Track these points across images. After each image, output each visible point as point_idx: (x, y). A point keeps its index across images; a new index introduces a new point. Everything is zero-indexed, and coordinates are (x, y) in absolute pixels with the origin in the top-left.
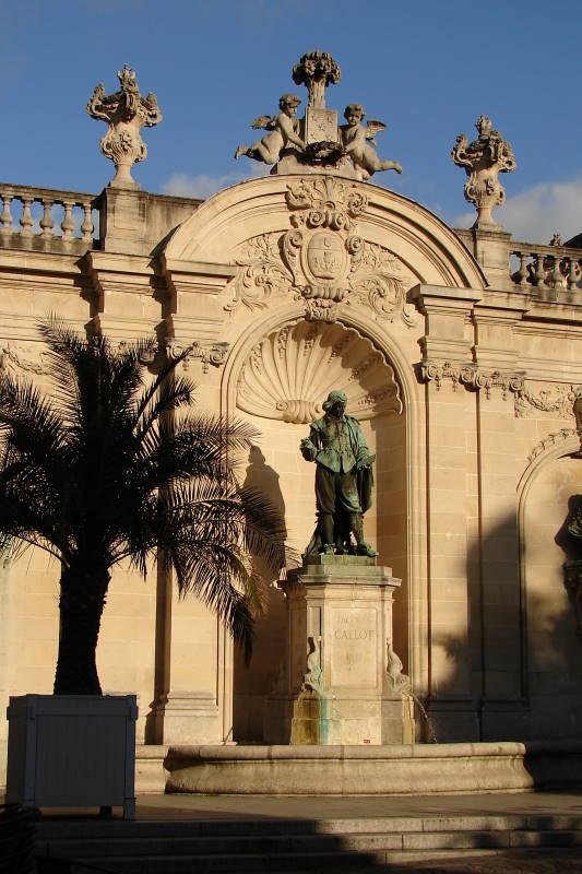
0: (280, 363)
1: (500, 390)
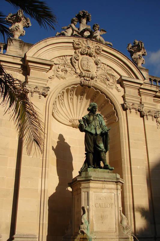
0: (71, 104)
1: (151, 117)
